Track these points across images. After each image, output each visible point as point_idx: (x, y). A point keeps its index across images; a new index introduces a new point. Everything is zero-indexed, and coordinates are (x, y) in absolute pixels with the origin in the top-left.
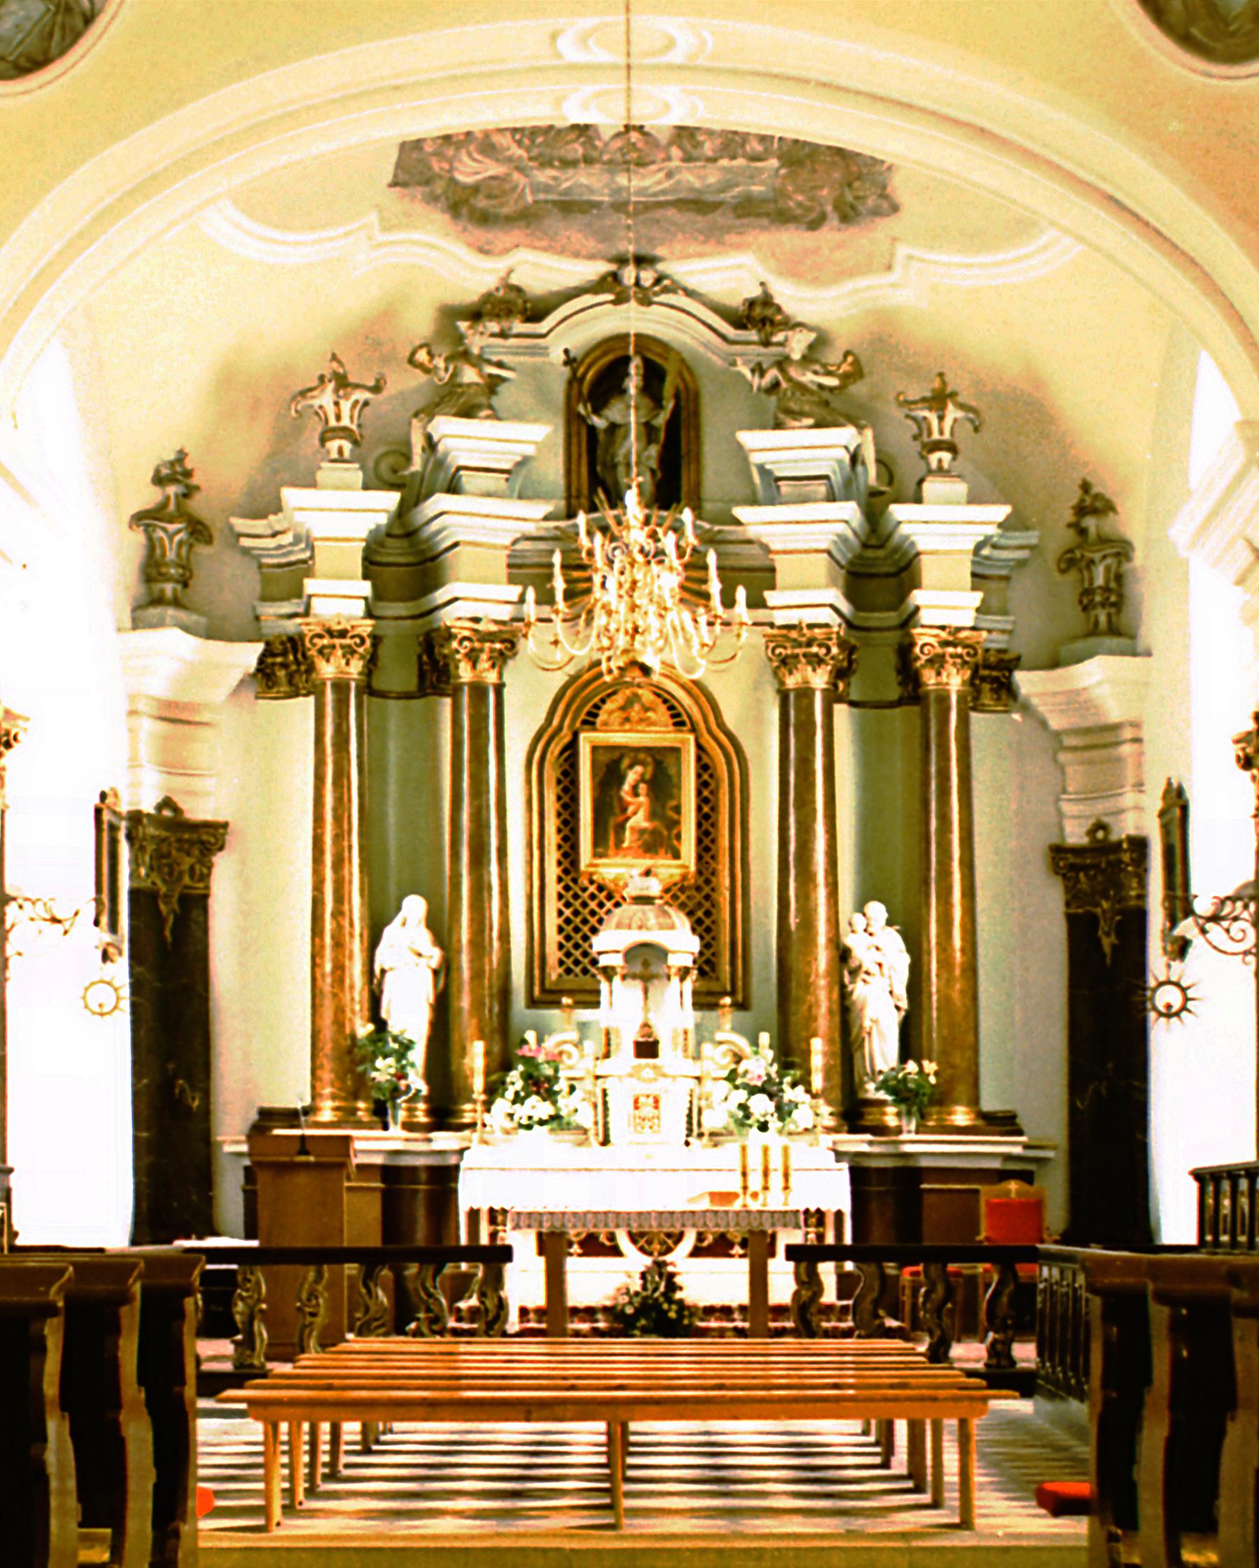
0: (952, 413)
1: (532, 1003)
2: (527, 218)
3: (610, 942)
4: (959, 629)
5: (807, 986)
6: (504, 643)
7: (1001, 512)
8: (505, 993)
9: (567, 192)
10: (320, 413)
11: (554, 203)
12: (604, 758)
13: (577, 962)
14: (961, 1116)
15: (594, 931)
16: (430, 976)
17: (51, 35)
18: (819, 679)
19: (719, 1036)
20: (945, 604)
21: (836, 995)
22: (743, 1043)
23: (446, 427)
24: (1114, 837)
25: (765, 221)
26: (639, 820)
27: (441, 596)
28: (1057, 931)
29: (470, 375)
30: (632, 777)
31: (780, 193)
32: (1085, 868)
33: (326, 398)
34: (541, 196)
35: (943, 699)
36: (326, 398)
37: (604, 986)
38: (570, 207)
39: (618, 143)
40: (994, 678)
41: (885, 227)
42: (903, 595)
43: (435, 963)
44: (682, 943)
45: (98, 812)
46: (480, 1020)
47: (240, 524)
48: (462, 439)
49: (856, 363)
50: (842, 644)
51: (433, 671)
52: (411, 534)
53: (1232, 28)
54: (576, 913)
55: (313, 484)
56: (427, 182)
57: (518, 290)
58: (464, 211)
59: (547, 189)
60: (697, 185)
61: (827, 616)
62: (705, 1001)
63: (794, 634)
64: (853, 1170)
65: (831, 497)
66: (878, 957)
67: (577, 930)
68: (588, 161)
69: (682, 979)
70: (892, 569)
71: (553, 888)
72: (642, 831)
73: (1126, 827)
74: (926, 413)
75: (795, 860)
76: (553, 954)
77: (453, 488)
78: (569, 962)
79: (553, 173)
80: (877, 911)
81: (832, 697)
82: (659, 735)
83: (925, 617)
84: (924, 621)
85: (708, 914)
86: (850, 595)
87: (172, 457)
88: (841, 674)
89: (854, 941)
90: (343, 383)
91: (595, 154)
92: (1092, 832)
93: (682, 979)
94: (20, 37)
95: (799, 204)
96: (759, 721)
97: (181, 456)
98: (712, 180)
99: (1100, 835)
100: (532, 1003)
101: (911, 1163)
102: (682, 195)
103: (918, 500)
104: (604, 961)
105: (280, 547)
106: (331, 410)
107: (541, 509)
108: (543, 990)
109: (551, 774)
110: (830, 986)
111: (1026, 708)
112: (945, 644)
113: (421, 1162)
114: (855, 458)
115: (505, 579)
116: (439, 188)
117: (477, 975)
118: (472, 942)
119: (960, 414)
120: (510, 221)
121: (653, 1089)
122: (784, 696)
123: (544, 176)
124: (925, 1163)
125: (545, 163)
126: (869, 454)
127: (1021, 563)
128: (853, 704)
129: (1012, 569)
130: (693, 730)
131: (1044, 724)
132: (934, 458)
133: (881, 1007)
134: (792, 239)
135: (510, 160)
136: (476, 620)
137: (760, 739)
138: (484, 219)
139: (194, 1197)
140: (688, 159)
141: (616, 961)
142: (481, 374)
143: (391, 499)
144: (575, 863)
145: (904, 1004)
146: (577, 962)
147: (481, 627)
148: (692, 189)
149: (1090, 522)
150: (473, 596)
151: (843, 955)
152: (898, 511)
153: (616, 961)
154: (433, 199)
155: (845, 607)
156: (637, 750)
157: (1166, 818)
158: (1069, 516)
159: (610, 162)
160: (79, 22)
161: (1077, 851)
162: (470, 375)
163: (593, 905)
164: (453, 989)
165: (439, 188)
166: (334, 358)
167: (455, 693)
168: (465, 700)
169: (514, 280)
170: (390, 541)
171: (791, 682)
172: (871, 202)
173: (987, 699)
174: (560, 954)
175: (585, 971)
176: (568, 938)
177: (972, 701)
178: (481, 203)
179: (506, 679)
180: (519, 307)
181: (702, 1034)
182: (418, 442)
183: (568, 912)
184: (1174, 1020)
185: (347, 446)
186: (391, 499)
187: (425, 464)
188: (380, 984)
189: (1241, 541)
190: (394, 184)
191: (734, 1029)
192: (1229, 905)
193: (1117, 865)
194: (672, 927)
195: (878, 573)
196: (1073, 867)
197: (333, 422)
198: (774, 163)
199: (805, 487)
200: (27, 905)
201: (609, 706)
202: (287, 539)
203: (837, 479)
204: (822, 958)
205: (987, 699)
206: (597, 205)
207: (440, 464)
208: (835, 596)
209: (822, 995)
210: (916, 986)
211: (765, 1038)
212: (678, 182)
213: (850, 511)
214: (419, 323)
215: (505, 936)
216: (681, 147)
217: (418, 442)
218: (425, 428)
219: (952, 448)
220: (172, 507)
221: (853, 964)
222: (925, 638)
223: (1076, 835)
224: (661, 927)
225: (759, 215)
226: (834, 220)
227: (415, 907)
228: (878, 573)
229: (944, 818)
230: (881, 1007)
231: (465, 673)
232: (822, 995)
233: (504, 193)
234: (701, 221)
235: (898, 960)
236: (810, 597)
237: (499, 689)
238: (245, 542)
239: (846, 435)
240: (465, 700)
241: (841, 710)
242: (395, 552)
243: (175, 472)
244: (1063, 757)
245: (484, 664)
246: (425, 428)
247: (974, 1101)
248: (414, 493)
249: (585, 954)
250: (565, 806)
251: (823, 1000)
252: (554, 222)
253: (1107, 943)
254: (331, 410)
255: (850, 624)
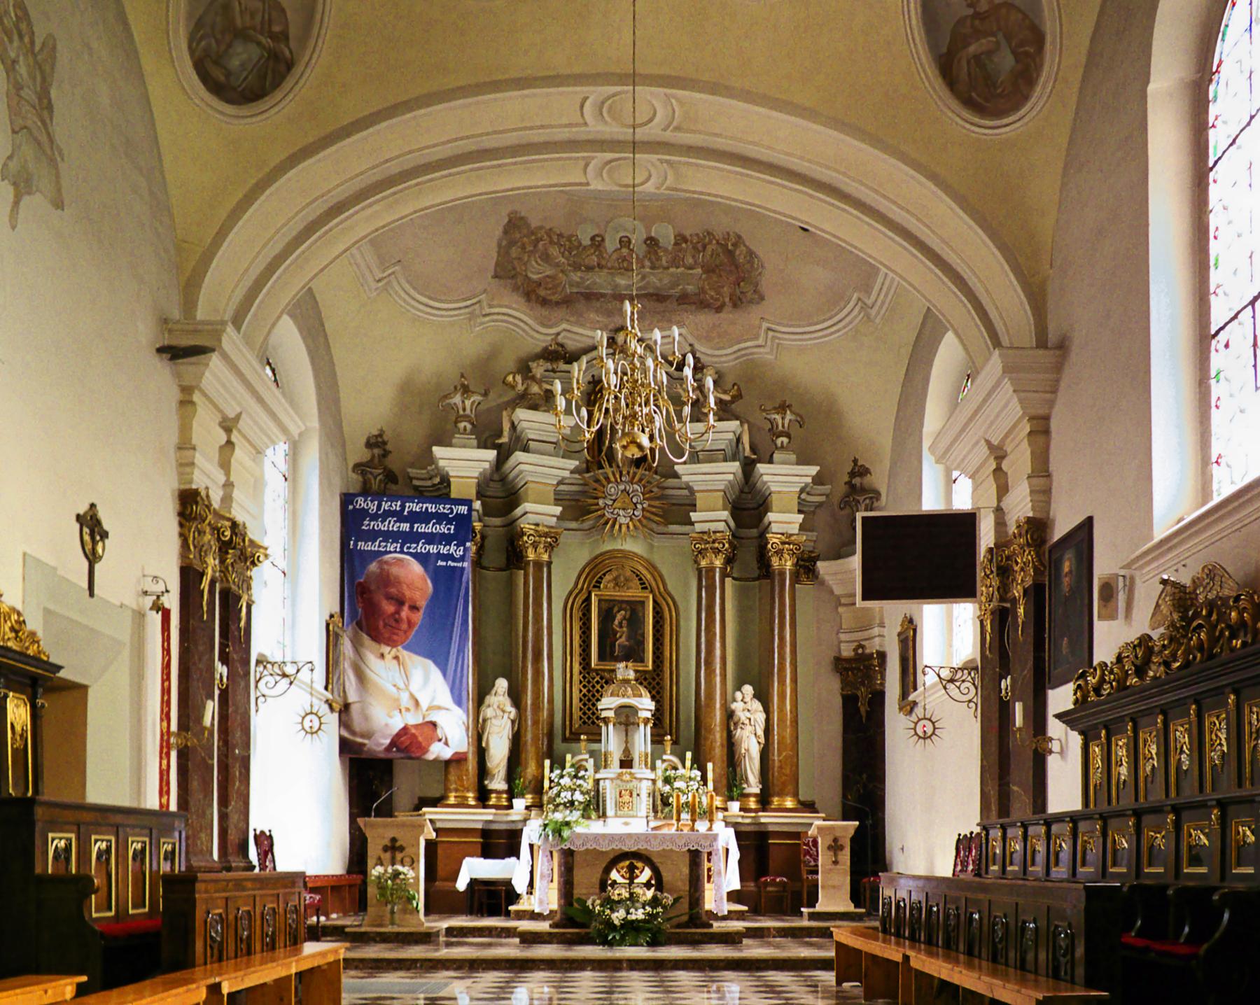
0: (789, 416)
1: (565, 740)
2: (567, 302)
3: (608, 704)
4: (792, 535)
5: (710, 731)
6: (552, 540)
7: (814, 470)
8: (550, 735)
9: (588, 287)
10: (453, 407)
11: (581, 294)
12: (605, 606)
13: (589, 718)
14: (789, 803)
15: (598, 700)
16: (509, 723)
17: (265, 78)
18: (718, 563)
19: (665, 757)
20: (784, 522)
21: (725, 735)
22: (675, 760)
23: (522, 414)
24: (868, 651)
25: (694, 307)
26: (622, 640)
27: (518, 511)
28: (838, 702)
29: (535, 389)
30: (619, 617)
31: (703, 290)
32: (852, 669)
33: (457, 399)
34: (575, 290)
35: (782, 573)
36: (457, 399)
37: (604, 729)
38: (590, 297)
39: (615, 256)
40: (806, 567)
41: (753, 315)
42: (761, 517)
43: (512, 716)
44: (645, 705)
45: (328, 625)
46: (537, 748)
47: (412, 472)
48: (529, 421)
49: (739, 389)
50: (730, 543)
51: (514, 556)
52: (503, 479)
53: (999, 91)
54: (589, 691)
55: (450, 445)
56: (513, 277)
57: (562, 346)
58: (533, 297)
59: (578, 285)
60: (658, 285)
61: (722, 526)
62: (657, 740)
63: (706, 537)
64: (736, 833)
65: (725, 460)
66: (748, 715)
67: (589, 700)
68: (600, 266)
69: (646, 725)
70: (755, 505)
71: (576, 677)
72: (625, 647)
73: (873, 647)
74: (776, 416)
75: (706, 661)
76: (577, 714)
77: (526, 449)
78: (585, 718)
79: (579, 274)
80: (748, 689)
81: (723, 570)
82: (634, 593)
83: (774, 528)
84: (774, 530)
85: (658, 693)
86: (733, 515)
87: (376, 433)
88: (729, 561)
89: (737, 706)
90: (466, 390)
91: (603, 263)
92: (855, 650)
93: (646, 725)
94: (245, 74)
95: (712, 297)
96: (686, 585)
97: (381, 430)
98: (666, 281)
99: (860, 651)
100: (565, 740)
101: (763, 829)
102: (651, 291)
103: (771, 461)
104: (604, 714)
105: (434, 485)
106: (460, 406)
107: (573, 464)
108: (571, 732)
109: (577, 614)
110: (722, 730)
111: (822, 583)
112: (783, 543)
113: (504, 827)
114: (738, 440)
115: (552, 501)
116: (519, 280)
117: (536, 723)
118: (533, 704)
119: (793, 417)
120: (557, 304)
121: (629, 786)
122: (699, 571)
123: (576, 277)
124: (771, 828)
125: (577, 267)
126: (746, 439)
127: (820, 505)
128: (734, 579)
129: (816, 507)
130: (652, 591)
131: (832, 592)
132: (779, 441)
133: (750, 744)
134: (705, 319)
135: (557, 265)
136: (537, 525)
137: (686, 598)
138: (544, 302)
139: (1187, 929)
140: (653, 268)
141: (611, 714)
142: (540, 387)
143: (491, 454)
144: (589, 664)
145: (762, 740)
146: (589, 718)
147: (540, 528)
148: (657, 288)
149: (857, 481)
150: (538, 512)
151: (730, 715)
152: (761, 468)
153: (611, 714)
154: (516, 288)
155: (732, 524)
156: (623, 602)
157: (903, 637)
158: (846, 479)
159: (612, 268)
160: (282, 68)
161: (847, 660)
162: (535, 389)
163: (598, 687)
164: (523, 731)
165: (519, 280)
166: (462, 376)
167: (525, 569)
168: (531, 570)
169: (560, 339)
170: (492, 484)
171: (703, 563)
172: (749, 295)
173: (803, 577)
174: (580, 713)
175: (593, 723)
176: (585, 705)
177: (796, 578)
178: (542, 292)
179: (554, 560)
180: (559, 356)
181: (656, 755)
182: (506, 427)
183: (584, 691)
184: (928, 741)
185: (469, 426)
186: (491, 454)
187: (510, 439)
188: (483, 728)
189: (983, 442)
190: (496, 276)
191: (672, 753)
192: (960, 673)
193: (869, 668)
194: (641, 696)
195: (749, 506)
196: (847, 669)
197: (461, 412)
198: (699, 271)
199: (711, 456)
200: (269, 666)
201: (608, 577)
202: (437, 480)
203: (729, 452)
204: (718, 715)
205: (803, 577)
206: (603, 295)
207: (518, 439)
208: (725, 514)
209: (718, 736)
210: (768, 731)
211: (689, 755)
212: (648, 283)
213: (735, 466)
214: (508, 361)
215: (551, 701)
216: (650, 259)
217: (506, 427)
218: (510, 416)
219: (788, 436)
220: (376, 460)
221: (735, 719)
222: (773, 539)
223: (847, 652)
224: (635, 696)
225: (690, 304)
226: (728, 307)
227: (502, 684)
228: (749, 506)
229: (782, 638)
230: (750, 744)
231: (531, 555)
232: (718, 736)
233: (555, 287)
234: (660, 307)
235: (761, 717)
236: (713, 518)
237: (549, 564)
238: (416, 483)
239: (734, 425)
240: (531, 570)
241: (728, 580)
242: (495, 489)
243: (376, 442)
244: (841, 609)
245: (541, 549)
246: (510, 416)
247: (795, 795)
248: (504, 454)
249: (593, 714)
250: (584, 633)
251: (718, 737)
252: (581, 305)
253: (863, 710)
254: (460, 406)
255: (733, 535)
